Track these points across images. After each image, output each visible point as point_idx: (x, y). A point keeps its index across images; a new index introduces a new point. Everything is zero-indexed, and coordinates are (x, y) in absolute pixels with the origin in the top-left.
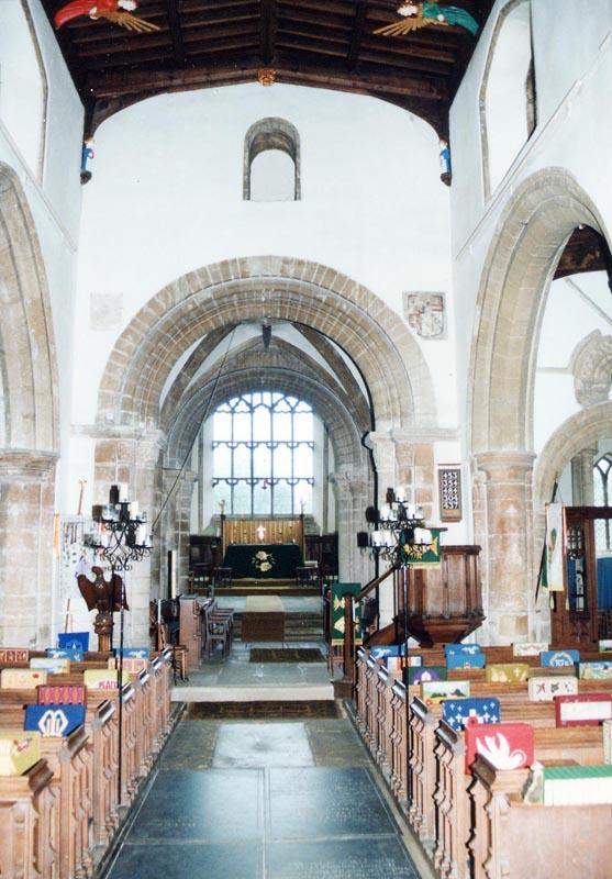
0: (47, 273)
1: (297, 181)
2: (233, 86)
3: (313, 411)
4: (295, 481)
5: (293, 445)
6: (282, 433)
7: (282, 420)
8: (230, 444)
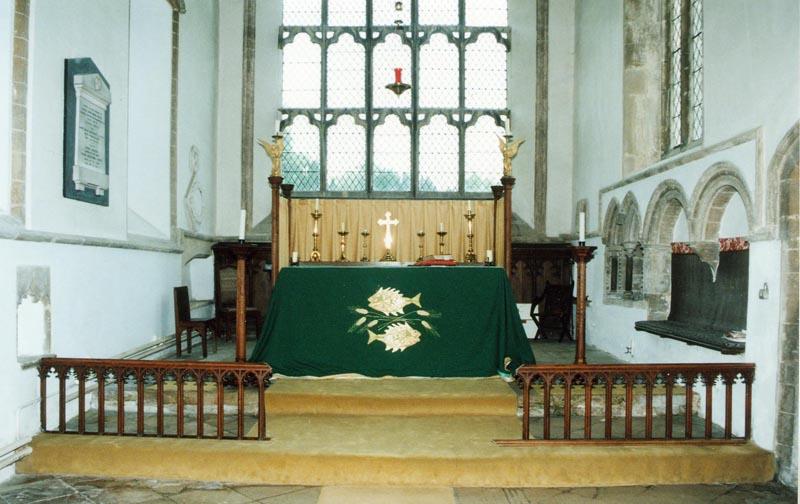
1: (462, 70)
4: (468, 118)
8: (319, 35)
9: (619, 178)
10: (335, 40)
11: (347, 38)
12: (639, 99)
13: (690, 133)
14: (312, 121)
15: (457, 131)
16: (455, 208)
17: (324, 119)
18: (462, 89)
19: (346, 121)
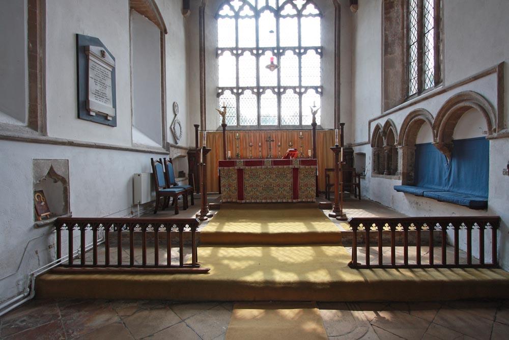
0: (32, 202)
1: (300, 67)
2: (220, 68)
3: (321, 15)
4: (303, 90)
5: (300, 51)
6: (289, 39)
7: (289, 26)
8: (235, 52)
9: (379, 114)
10: (242, 54)
11: (247, 53)
12: (391, 71)
13: (423, 86)
14: (233, 93)
15: (298, 97)
16: (112, 251)
17: (238, 91)
18: (300, 77)
19: (248, 93)
